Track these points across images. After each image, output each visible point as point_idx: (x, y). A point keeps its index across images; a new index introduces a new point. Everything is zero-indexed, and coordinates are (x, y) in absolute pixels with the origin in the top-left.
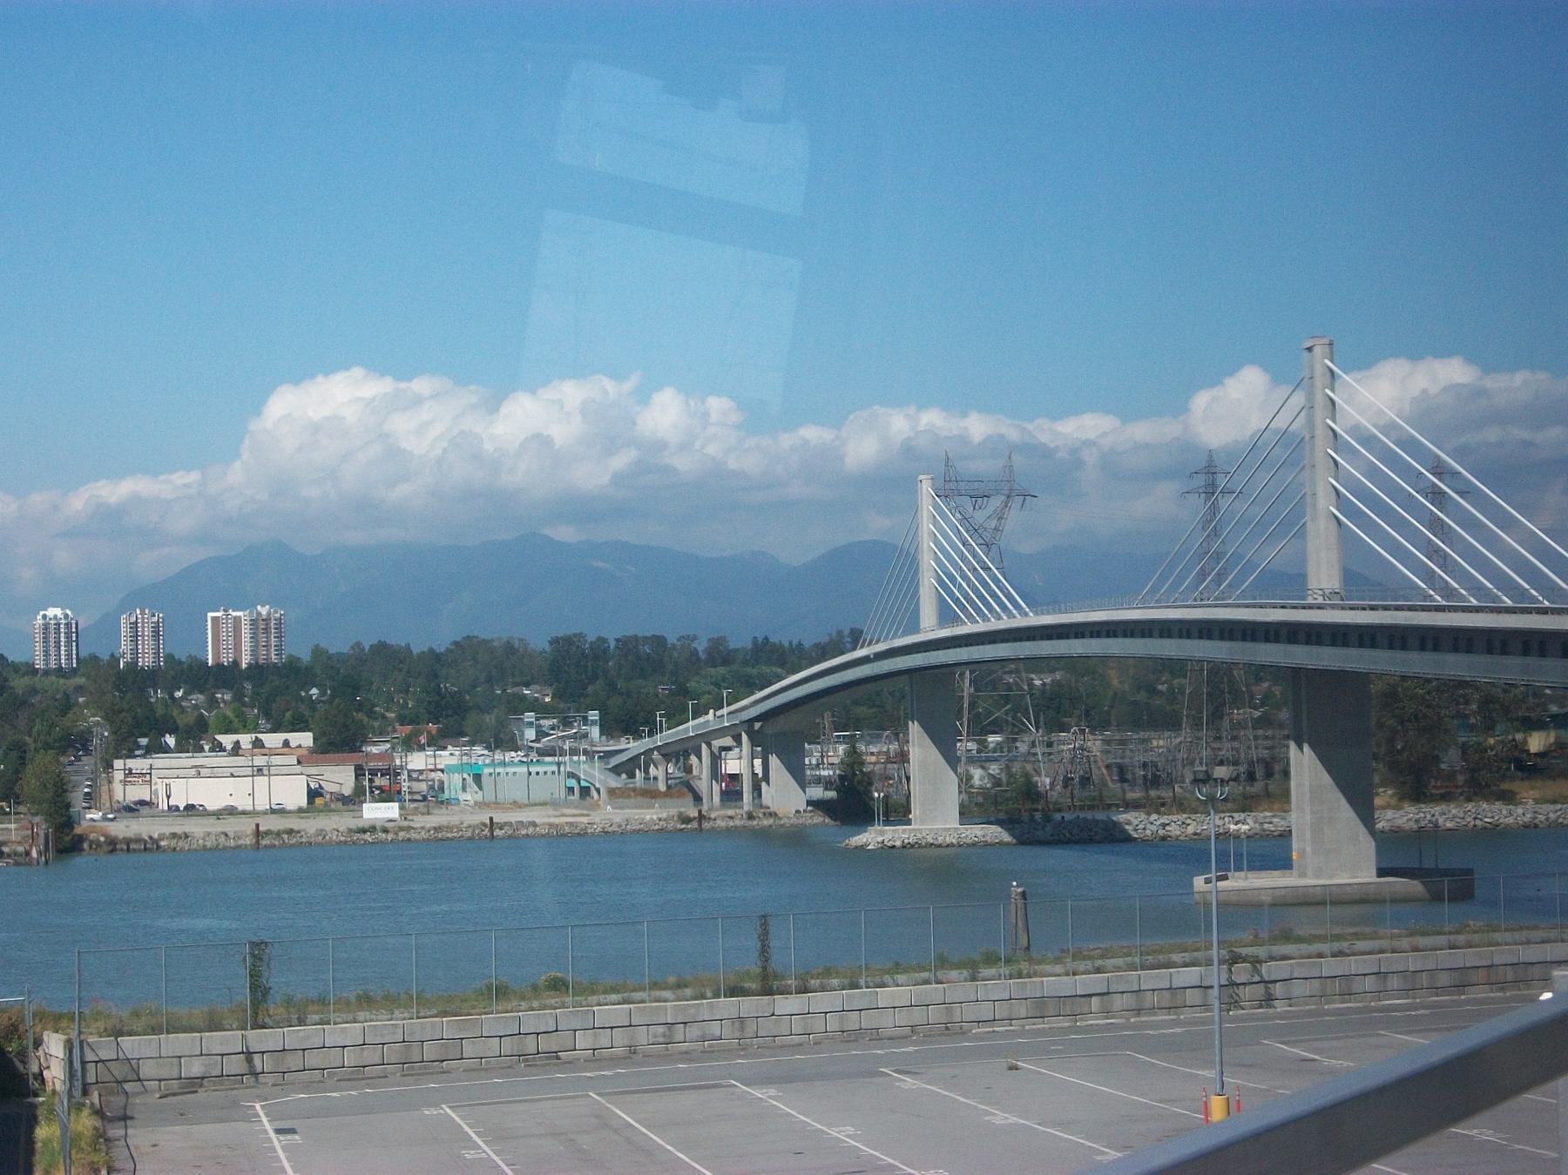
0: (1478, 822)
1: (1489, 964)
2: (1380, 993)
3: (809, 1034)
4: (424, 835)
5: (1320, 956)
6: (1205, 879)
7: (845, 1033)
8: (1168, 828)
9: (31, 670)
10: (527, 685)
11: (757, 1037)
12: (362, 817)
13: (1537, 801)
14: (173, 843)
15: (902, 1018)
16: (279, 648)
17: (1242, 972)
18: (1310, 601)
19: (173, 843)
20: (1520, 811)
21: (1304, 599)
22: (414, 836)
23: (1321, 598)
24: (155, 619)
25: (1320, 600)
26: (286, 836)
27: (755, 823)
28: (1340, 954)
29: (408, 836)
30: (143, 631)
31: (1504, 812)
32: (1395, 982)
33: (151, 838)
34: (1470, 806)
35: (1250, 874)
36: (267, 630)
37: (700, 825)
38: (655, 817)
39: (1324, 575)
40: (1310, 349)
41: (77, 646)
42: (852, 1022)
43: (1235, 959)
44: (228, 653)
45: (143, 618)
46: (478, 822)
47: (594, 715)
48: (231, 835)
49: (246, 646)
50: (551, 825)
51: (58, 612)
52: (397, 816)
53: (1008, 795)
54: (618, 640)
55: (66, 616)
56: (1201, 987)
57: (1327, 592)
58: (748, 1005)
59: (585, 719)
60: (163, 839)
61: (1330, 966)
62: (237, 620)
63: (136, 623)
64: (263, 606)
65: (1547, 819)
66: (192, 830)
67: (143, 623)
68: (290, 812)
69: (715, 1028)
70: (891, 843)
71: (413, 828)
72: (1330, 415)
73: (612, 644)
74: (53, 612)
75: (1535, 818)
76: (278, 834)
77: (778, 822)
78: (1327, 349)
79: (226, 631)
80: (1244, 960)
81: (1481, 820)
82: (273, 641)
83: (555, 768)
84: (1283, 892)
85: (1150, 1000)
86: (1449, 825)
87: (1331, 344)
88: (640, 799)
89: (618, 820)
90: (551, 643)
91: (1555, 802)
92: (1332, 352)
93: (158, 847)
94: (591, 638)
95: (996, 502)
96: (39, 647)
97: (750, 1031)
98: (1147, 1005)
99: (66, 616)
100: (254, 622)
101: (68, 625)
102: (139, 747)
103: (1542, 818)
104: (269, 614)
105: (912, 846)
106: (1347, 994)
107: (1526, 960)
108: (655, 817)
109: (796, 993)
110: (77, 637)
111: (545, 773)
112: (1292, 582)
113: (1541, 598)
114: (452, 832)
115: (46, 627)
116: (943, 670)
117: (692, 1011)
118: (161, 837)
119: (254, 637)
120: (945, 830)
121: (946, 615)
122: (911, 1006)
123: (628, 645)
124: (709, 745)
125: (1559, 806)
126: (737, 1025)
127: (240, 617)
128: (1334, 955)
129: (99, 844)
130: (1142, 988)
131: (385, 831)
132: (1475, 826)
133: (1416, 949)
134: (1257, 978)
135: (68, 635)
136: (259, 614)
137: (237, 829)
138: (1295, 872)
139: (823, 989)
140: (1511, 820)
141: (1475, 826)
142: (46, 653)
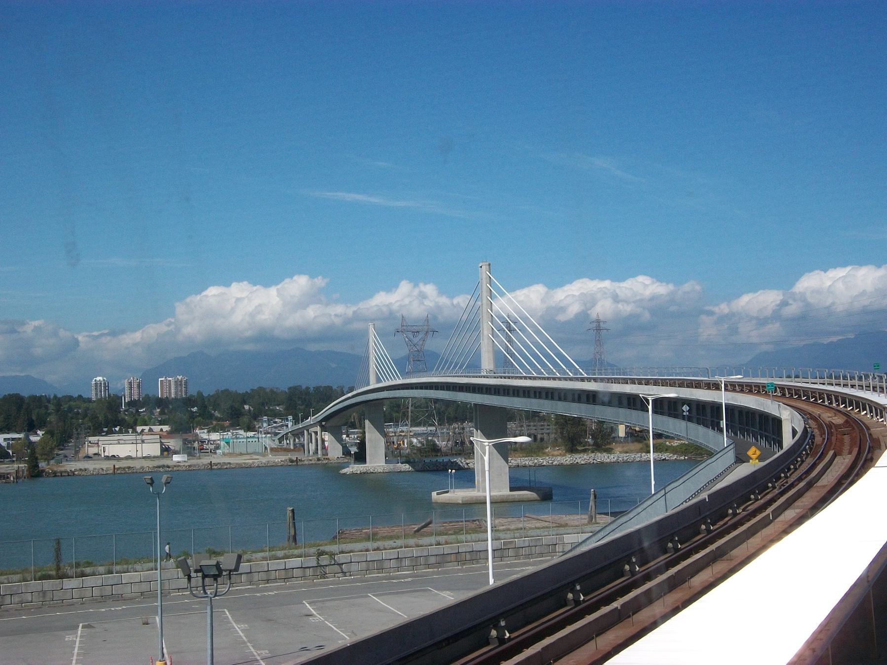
0: (595, 461)
1: (471, 550)
2: (398, 569)
3: (83, 598)
4: (184, 468)
5: (367, 550)
6: (437, 493)
7: (103, 597)
8: (469, 465)
9: (89, 400)
10: (278, 405)
11: (53, 600)
12: (172, 460)
13: (621, 452)
14: (80, 473)
15: (135, 588)
16: (186, 394)
17: (325, 560)
18: (482, 374)
19: (80, 473)
20: (612, 456)
21: (480, 373)
22: (180, 468)
23: (485, 373)
24: (138, 381)
25: (485, 374)
26: (127, 469)
27: (320, 462)
28: (378, 549)
29: (178, 469)
30: (134, 386)
31: (606, 457)
32: (407, 562)
33: (71, 471)
34: (593, 455)
35: (456, 490)
36: (181, 385)
37: (297, 463)
38: (279, 460)
39: (487, 363)
40: (481, 267)
41: (108, 391)
42: (108, 591)
43: (321, 554)
44: (166, 394)
45: (133, 381)
46: (207, 463)
47: (290, 418)
48: (105, 469)
49: (173, 391)
50: (237, 464)
51: (101, 378)
52: (186, 460)
53: (427, 450)
54: (314, 388)
55: (104, 380)
56: (302, 567)
57: (488, 370)
58: (48, 584)
59: (287, 419)
60: (76, 472)
61: (372, 556)
62: (170, 381)
63: (131, 382)
64: (179, 376)
65: (623, 460)
66: (88, 467)
67: (134, 383)
68: (122, 459)
69: (29, 597)
70: (356, 472)
71: (180, 466)
72: (489, 295)
73: (312, 389)
74: (98, 378)
75: (618, 459)
76: (124, 469)
77: (329, 462)
78: (488, 267)
79: (166, 385)
80: (327, 554)
81: (596, 460)
82: (183, 389)
83: (257, 440)
84: (467, 499)
85: (273, 575)
86: (582, 462)
87: (489, 265)
88: (282, 453)
89: (264, 461)
90: (288, 389)
91: (627, 452)
92: (490, 268)
93: (74, 474)
94: (304, 387)
95: (421, 336)
96: (93, 392)
97: (48, 598)
98: (273, 577)
99: (104, 380)
100: (176, 382)
101: (105, 384)
102: (104, 432)
103: (621, 459)
104: (182, 379)
105: (364, 473)
106: (381, 569)
107: (476, 550)
108: (279, 460)
109: (76, 578)
110: (108, 388)
111: (252, 441)
112: (474, 366)
113: (545, 373)
114: (196, 467)
115: (96, 384)
116: (377, 402)
117: (15, 588)
118: (76, 470)
119: (176, 388)
120: (378, 466)
121: (379, 380)
122: (141, 582)
123: (317, 389)
124: (308, 431)
125: (628, 454)
126: (41, 594)
127: (171, 380)
128: (374, 550)
129: (49, 473)
130: (269, 570)
131: (168, 467)
132: (593, 463)
133: (418, 546)
134: (333, 562)
135: (105, 387)
136: (178, 379)
137: (107, 466)
138: (476, 490)
139: (93, 574)
140: (608, 460)
141: (593, 463)
142: (96, 394)
